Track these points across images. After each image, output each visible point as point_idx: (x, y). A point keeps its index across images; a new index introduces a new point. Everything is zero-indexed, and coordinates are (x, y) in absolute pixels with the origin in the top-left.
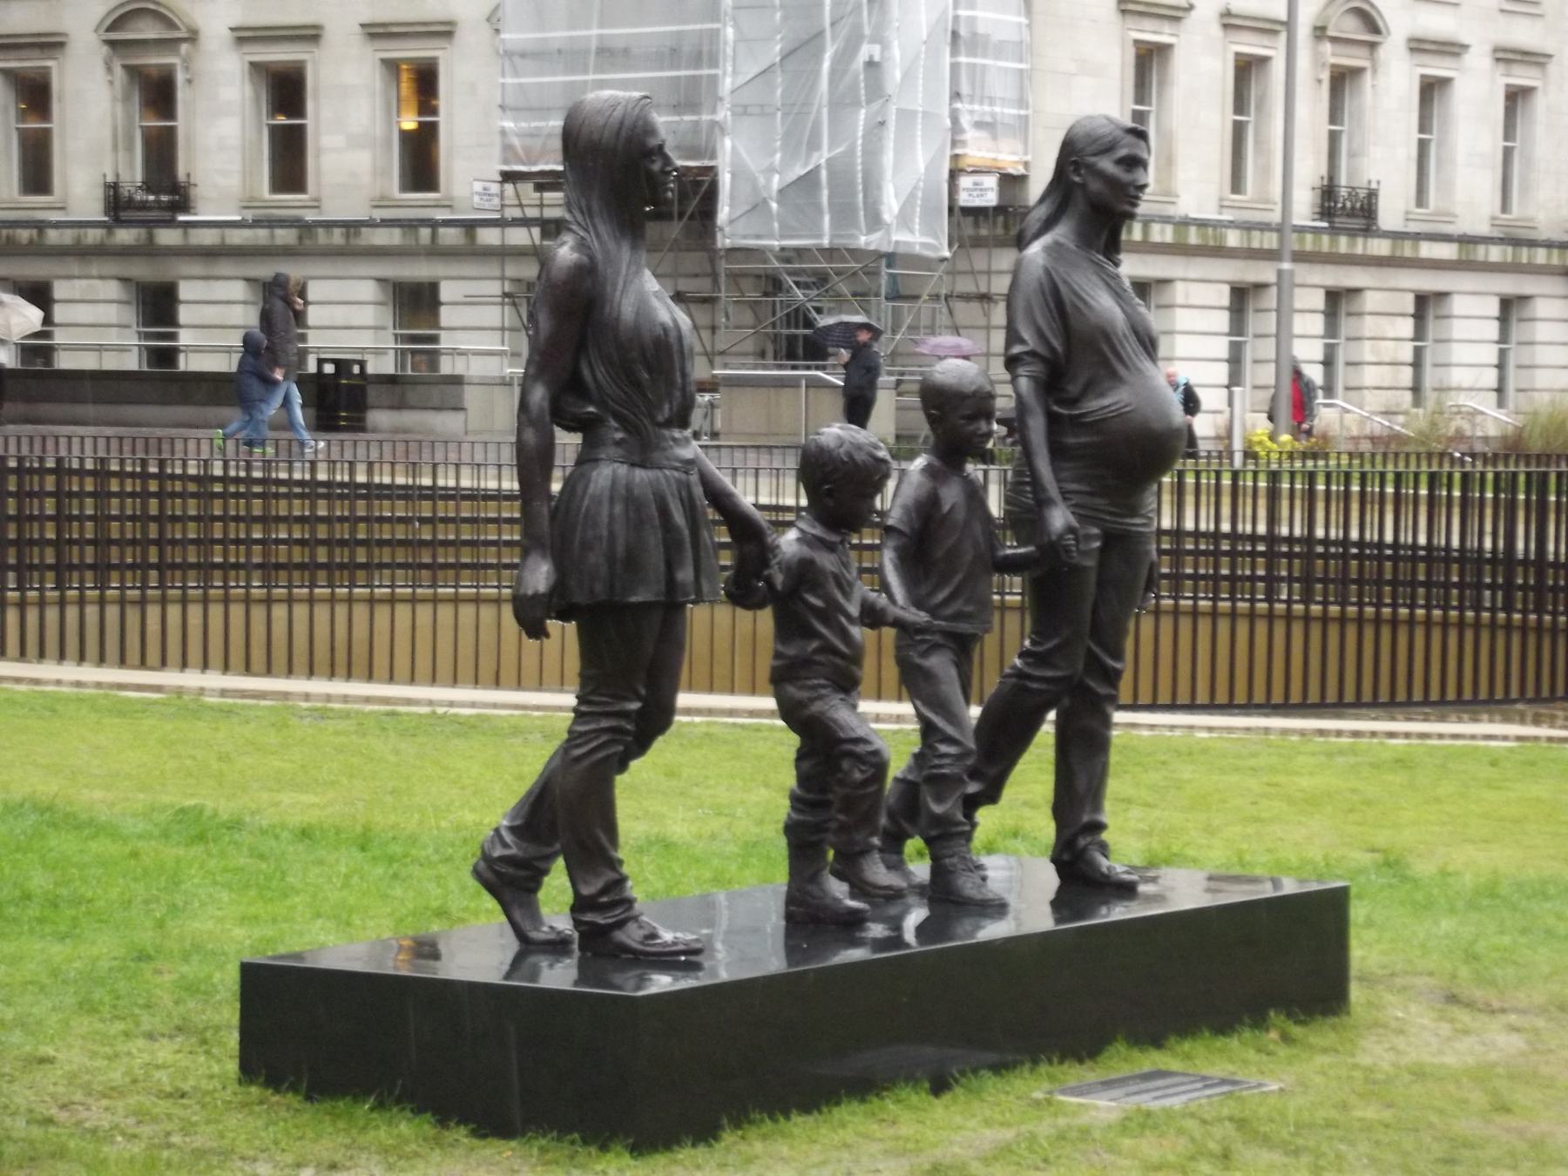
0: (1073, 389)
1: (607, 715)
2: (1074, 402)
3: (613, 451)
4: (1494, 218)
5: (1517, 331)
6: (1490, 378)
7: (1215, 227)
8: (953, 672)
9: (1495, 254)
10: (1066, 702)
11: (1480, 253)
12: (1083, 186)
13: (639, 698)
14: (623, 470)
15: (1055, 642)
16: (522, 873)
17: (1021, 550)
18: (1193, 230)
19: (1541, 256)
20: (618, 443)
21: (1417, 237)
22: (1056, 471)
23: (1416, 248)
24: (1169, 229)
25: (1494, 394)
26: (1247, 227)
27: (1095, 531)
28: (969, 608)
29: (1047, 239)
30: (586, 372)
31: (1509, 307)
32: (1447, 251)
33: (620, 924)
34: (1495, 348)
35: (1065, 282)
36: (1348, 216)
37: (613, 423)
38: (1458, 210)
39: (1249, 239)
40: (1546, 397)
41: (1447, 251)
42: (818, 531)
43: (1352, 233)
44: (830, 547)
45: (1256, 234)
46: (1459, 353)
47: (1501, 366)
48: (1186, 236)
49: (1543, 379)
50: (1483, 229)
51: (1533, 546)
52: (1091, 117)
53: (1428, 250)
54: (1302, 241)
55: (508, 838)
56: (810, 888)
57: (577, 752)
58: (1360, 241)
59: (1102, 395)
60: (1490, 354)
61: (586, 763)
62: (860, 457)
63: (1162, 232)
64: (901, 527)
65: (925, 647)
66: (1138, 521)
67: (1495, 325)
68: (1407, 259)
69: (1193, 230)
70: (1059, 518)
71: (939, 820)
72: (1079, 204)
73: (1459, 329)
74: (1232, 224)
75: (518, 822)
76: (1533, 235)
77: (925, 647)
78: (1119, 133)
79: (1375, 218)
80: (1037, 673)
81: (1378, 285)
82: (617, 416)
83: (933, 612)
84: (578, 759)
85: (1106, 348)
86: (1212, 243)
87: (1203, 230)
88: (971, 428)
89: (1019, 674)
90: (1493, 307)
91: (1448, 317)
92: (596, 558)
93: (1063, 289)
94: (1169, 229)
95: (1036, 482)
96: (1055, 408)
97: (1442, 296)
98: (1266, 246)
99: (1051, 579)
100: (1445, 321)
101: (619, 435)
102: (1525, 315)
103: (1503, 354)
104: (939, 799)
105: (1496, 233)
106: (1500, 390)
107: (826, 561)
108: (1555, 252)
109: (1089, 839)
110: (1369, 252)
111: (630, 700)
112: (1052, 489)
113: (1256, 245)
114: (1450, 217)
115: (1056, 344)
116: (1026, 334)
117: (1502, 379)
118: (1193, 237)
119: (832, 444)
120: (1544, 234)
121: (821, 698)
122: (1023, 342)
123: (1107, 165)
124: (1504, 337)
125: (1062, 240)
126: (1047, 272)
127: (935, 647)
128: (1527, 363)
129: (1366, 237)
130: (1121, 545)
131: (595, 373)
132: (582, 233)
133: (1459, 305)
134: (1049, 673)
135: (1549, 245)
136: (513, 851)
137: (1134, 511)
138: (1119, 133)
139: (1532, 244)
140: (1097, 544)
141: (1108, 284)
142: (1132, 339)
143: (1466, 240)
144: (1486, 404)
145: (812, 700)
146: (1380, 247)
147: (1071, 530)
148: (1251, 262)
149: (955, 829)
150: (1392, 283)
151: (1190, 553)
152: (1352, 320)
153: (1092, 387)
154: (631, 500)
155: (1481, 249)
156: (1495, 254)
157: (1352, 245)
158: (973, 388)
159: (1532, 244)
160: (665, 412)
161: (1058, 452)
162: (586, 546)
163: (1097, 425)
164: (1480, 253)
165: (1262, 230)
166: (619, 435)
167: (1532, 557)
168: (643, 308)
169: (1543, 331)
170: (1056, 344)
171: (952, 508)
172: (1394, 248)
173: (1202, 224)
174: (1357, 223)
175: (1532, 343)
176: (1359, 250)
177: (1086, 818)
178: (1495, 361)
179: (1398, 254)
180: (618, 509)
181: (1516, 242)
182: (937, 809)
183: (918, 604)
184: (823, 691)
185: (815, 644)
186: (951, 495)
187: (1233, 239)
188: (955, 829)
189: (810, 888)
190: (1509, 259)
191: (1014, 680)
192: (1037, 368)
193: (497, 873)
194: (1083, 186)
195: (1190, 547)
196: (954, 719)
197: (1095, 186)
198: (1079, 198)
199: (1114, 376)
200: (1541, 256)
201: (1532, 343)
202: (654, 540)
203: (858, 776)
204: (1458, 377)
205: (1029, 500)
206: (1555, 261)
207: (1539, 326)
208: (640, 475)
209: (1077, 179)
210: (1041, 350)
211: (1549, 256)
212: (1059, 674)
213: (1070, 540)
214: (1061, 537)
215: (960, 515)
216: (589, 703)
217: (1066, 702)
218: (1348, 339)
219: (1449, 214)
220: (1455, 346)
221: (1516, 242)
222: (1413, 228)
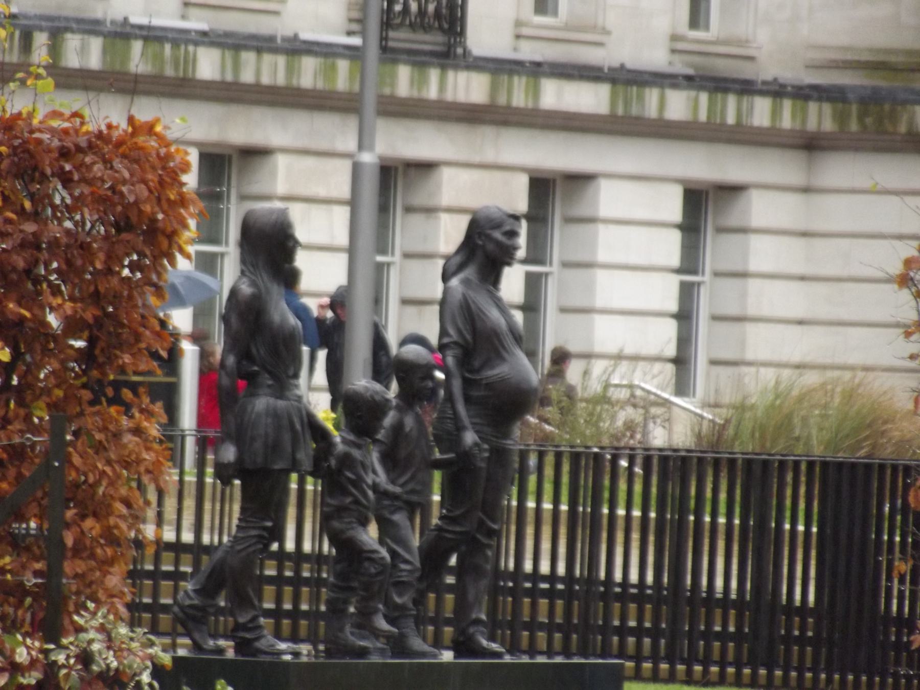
0: (477, 364)
1: (254, 528)
2: (478, 371)
3: (267, 391)
4: (675, 38)
5: (717, 251)
6: (663, 336)
7: (176, 43)
8: (408, 523)
9: (678, 105)
10: (463, 548)
11: (651, 103)
12: (483, 247)
13: (272, 520)
14: (272, 400)
15: (462, 510)
16: (200, 614)
17: (445, 456)
18: (137, 46)
19: (761, 112)
20: (269, 386)
21: (537, 70)
22: (468, 410)
23: (536, 93)
24: (96, 44)
25: (670, 368)
26: (233, 43)
27: (486, 446)
28: (418, 488)
29: (461, 276)
30: (254, 351)
31: (702, 206)
32: (589, 99)
33: (258, 639)
34: (674, 281)
35: (474, 302)
36: (412, 26)
37: (267, 376)
38: (611, 20)
39: (237, 66)
40: (768, 375)
41: (589, 99)
42: (351, 437)
43: (420, 60)
44: (359, 447)
45: (248, 57)
46: (610, 289)
47: (684, 316)
48: (126, 57)
49: (761, 343)
50: (657, 57)
51: (734, 584)
52: (487, 207)
53: (556, 95)
54: (330, 71)
55: (192, 594)
56: (340, 634)
57: (239, 548)
58: (434, 74)
59: (493, 368)
60: (664, 293)
61: (244, 554)
62: (377, 398)
63: (83, 51)
64: (383, 439)
65: (393, 509)
66: (509, 442)
67: (675, 238)
68: (518, 111)
69: (137, 46)
70: (470, 437)
71: (397, 607)
72: (479, 254)
73: (609, 243)
74: (206, 38)
75: (198, 587)
76: (746, 71)
77: (393, 509)
78: (504, 217)
79: (462, 33)
80: (450, 528)
81: (462, 156)
82: (270, 373)
83: (402, 486)
84: (240, 551)
85: (497, 342)
86: (169, 72)
87: (153, 47)
88: (423, 384)
89: (439, 529)
90: (671, 206)
91: (592, 220)
92: (258, 445)
93: (473, 306)
94: (96, 44)
95: (456, 417)
96: (467, 375)
97: (579, 181)
98: (266, 80)
99: (460, 475)
100: (591, 226)
101: (270, 382)
102: (733, 220)
103: (687, 293)
104: (400, 595)
105: (680, 67)
106: (682, 362)
107: (356, 453)
108: (787, 105)
109: (476, 628)
110: (449, 96)
111: (267, 521)
112: (466, 421)
113: (247, 76)
114: (598, 33)
115: (469, 337)
116: (452, 331)
117: (685, 340)
118: (137, 59)
119: (362, 390)
120: (769, 69)
121: (353, 528)
122: (448, 335)
123: (497, 235)
124: (691, 261)
125: (471, 277)
126: (464, 295)
127: (398, 509)
128: (733, 311)
129: (443, 68)
130: (499, 455)
131: (260, 351)
132: (254, 278)
133: (610, 199)
134: (458, 529)
135: (777, 91)
136: (196, 602)
137: (507, 435)
138: (504, 217)
139: (747, 88)
140: (486, 455)
141: (495, 302)
142: (510, 336)
143: (625, 79)
144: (655, 381)
145: (348, 529)
146: (470, 88)
147: (476, 444)
148: (234, 108)
149: (408, 613)
150: (489, 156)
151: (270, 580)
152: (416, 220)
153: (488, 363)
154: (275, 414)
155: (652, 96)
156: (678, 105)
157: (420, 81)
158: (425, 362)
159: (747, 88)
160: (291, 372)
161: (468, 400)
162: (253, 439)
163: (489, 386)
164: (651, 103)
165: (259, 51)
166: (270, 382)
167: (733, 596)
168: (284, 319)
169: (762, 254)
170: (469, 337)
171: (411, 430)
172: (494, 89)
173: (152, 36)
174: (432, 40)
175: (744, 275)
176: (432, 92)
177: (474, 616)
178: (673, 306)
179: (502, 100)
180: (269, 420)
181: (719, 85)
182: (398, 600)
183: (393, 482)
184: (355, 525)
185: (349, 500)
186: (409, 422)
187: (208, 65)
188: (408, 613)
189: (340, 634)
190: (703, 116)
191: (436, 533)
192: (458, 351)
193: (185, 613)
194: (483, 247)
195: (271, 572)
196: (408, 548)
197: (490, 247)
198: (479, 254)
199: (503, 359)
200: (761, 112)
201: (744, 275)
202: (287, 437)
203: (373, 570)
204: (607, 334)
205: (450, 426)
206: (787, 122)
207: (756, 242)
208: (281, 403)
209: (480, 243)
210: (460, 341)
211: (776, 113)
212: (463, 529)
213: (476, 451)
214: (471, 448)
215: (415, 433)
216: (247, 522)
217: (463, 548)
218: (407, 256)
219: (594, 28)
220: (601, 275)
221: (719, 85)
222: (529, 52)
